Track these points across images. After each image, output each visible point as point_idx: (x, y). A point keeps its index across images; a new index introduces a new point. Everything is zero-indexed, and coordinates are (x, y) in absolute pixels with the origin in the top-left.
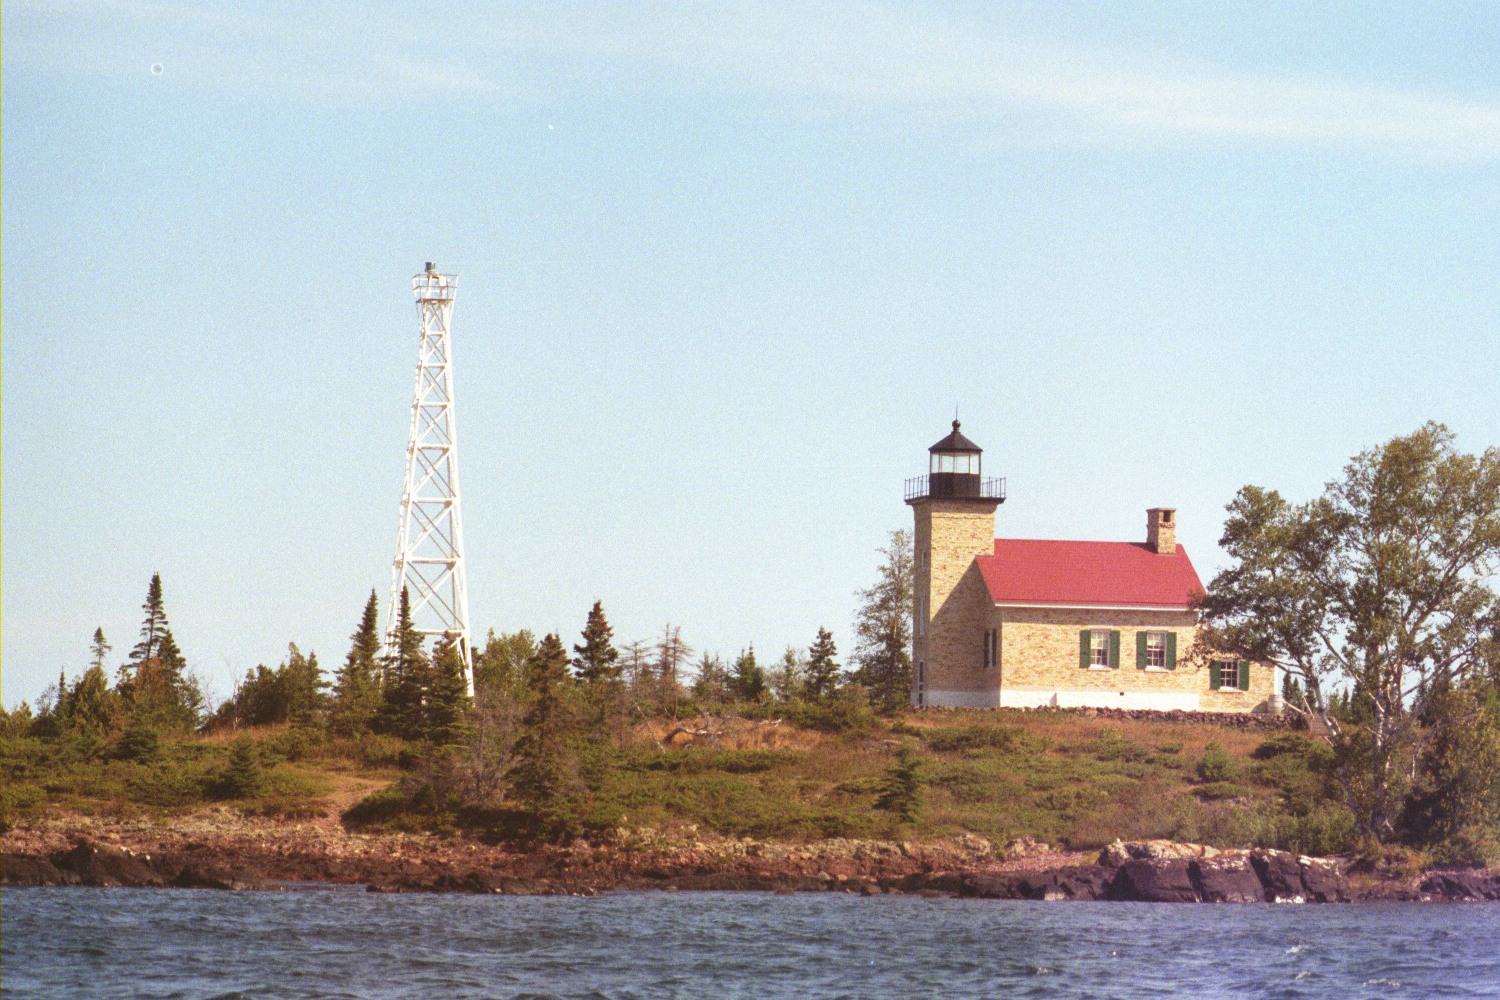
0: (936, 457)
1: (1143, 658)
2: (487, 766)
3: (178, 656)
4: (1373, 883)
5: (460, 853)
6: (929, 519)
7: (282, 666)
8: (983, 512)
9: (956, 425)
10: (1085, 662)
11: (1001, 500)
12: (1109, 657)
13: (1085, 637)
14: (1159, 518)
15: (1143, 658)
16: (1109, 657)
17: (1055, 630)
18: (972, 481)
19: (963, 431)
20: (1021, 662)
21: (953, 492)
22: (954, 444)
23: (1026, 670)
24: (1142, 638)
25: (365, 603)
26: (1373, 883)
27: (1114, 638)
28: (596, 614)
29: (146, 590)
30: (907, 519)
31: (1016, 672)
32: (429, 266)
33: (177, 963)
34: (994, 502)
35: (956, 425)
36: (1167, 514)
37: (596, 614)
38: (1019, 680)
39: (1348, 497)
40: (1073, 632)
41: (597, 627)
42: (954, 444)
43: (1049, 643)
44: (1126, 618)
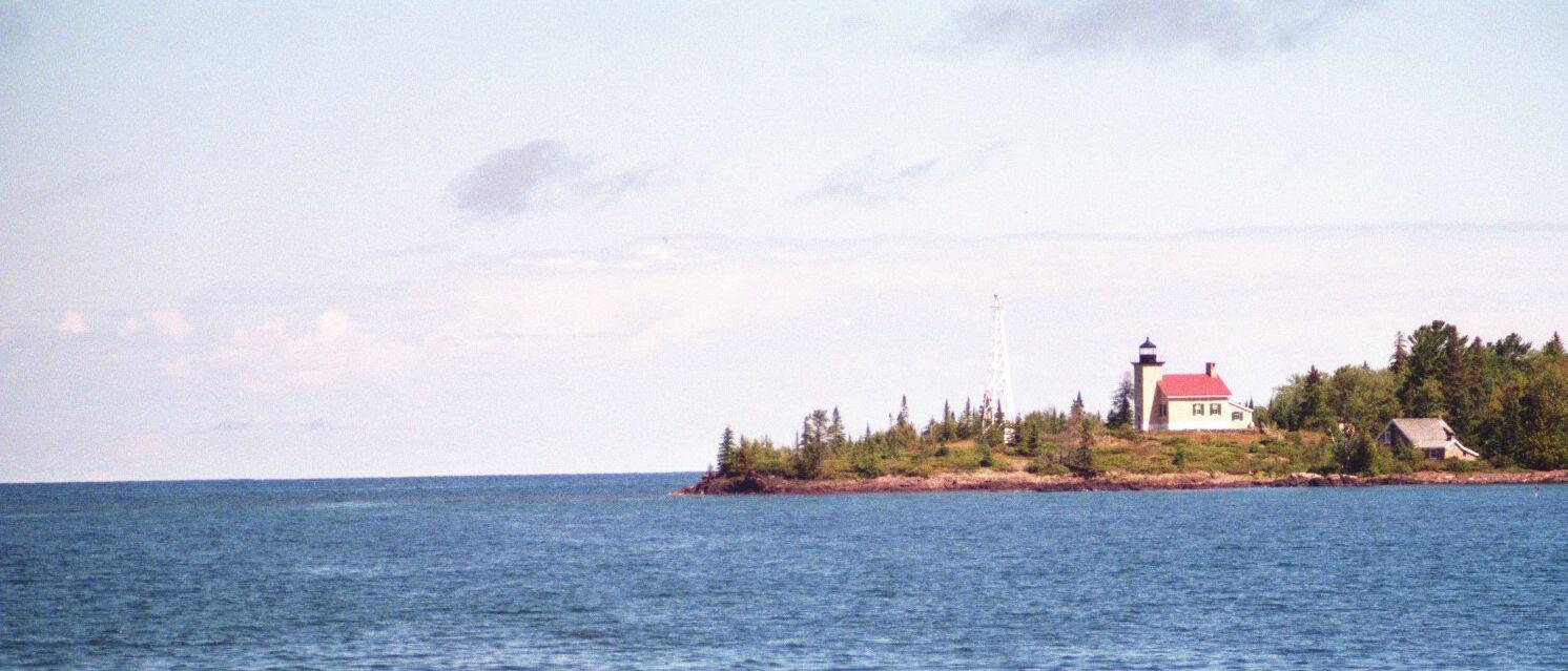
1: (1212, 411)
4: (1425, 662)
5: (668, 647)
6: (1141, 371)
7: (1499, 341)
10: (1194, 412)
12: (1202, 412)
13: (1194, 406)
14: (1209, 366)
15: (1212, 411)
16: (1202, 412)
21: (1148, 360)
24: (1211, 405)
25: (966, 401)
26: (1425, 662)
27: (1202, 406)
29: (901, 400)
30: (1132, 369)
32: (995, 296)
36: (1214, 365)
39: (802, 575)
40: (1191, 404)
42: (1147, 345)
44: (1206, 399)
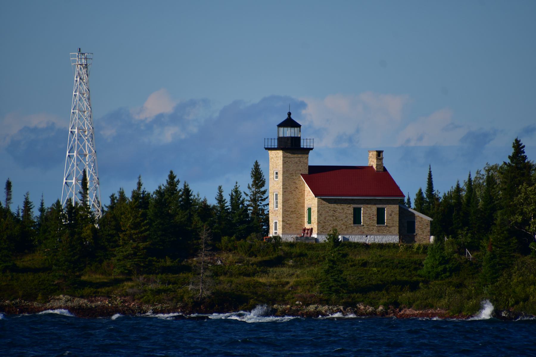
0: (281, 129)
2: (171, 230)
3: (447, 195)
8: (304, 154)
9: (289, 114)
11: (312, 149)
17: (345, 206)
18: (296, 140)
19: (292, 116)
20: (325, 222)
22: (289, 123)
23: (327, 226)
28: (256, 162)
31: (323, 227)
33: (142, 257)
34: (307, 151)
35: (289, 114)
37: (256, 162)
38: (324, 231)
41: (524, 146)
42: (289, 123)
43: (337, 214)
